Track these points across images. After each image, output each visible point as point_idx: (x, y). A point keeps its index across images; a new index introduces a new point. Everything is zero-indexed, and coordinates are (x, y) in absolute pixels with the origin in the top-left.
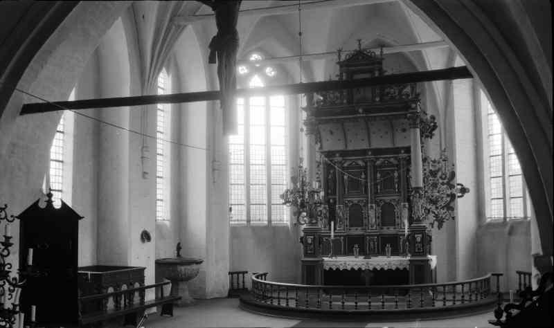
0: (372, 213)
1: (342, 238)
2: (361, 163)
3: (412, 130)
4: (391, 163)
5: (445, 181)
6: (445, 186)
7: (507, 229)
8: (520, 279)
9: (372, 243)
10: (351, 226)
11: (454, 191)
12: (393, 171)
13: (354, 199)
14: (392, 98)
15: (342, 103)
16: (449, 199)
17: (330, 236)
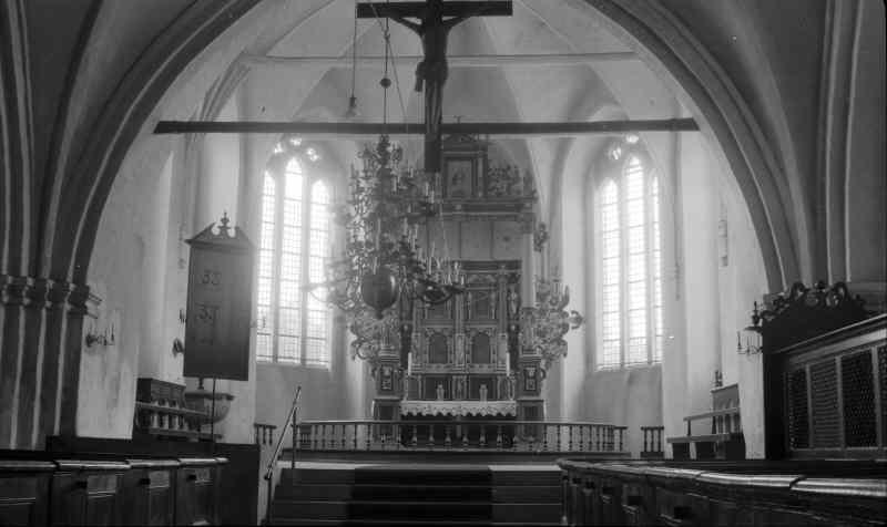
1: (420, 377)
3: (525, 235)
5: (556, 308)
6: (555, 314)
7: (626, 377)
8: (646, 436)
9: (459, 386)
10: (432, 362)
13: (435, 327)
14: (499, 194)
16: (560, 331)
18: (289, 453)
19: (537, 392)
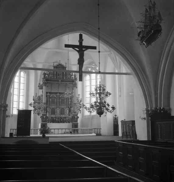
2: (55, 96)
11: (81, 106)
14: (69, 78)
18: (131, 138)
19: (77, 121)
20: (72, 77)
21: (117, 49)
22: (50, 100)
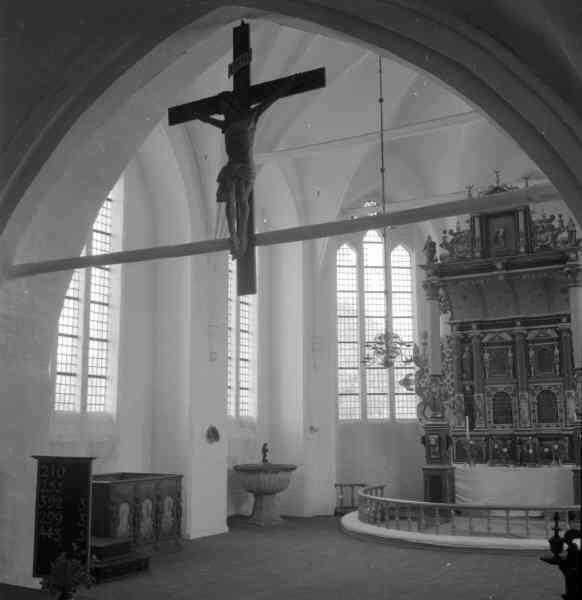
0: (524, 405)
1: (483, 439)
4: (549, 335)
10: (496, 422)
12: (553, 347)
15: (474, 258)
17: (464, 436)
20: (560, 237)
21: (459, 67)
22: (486, 356)
